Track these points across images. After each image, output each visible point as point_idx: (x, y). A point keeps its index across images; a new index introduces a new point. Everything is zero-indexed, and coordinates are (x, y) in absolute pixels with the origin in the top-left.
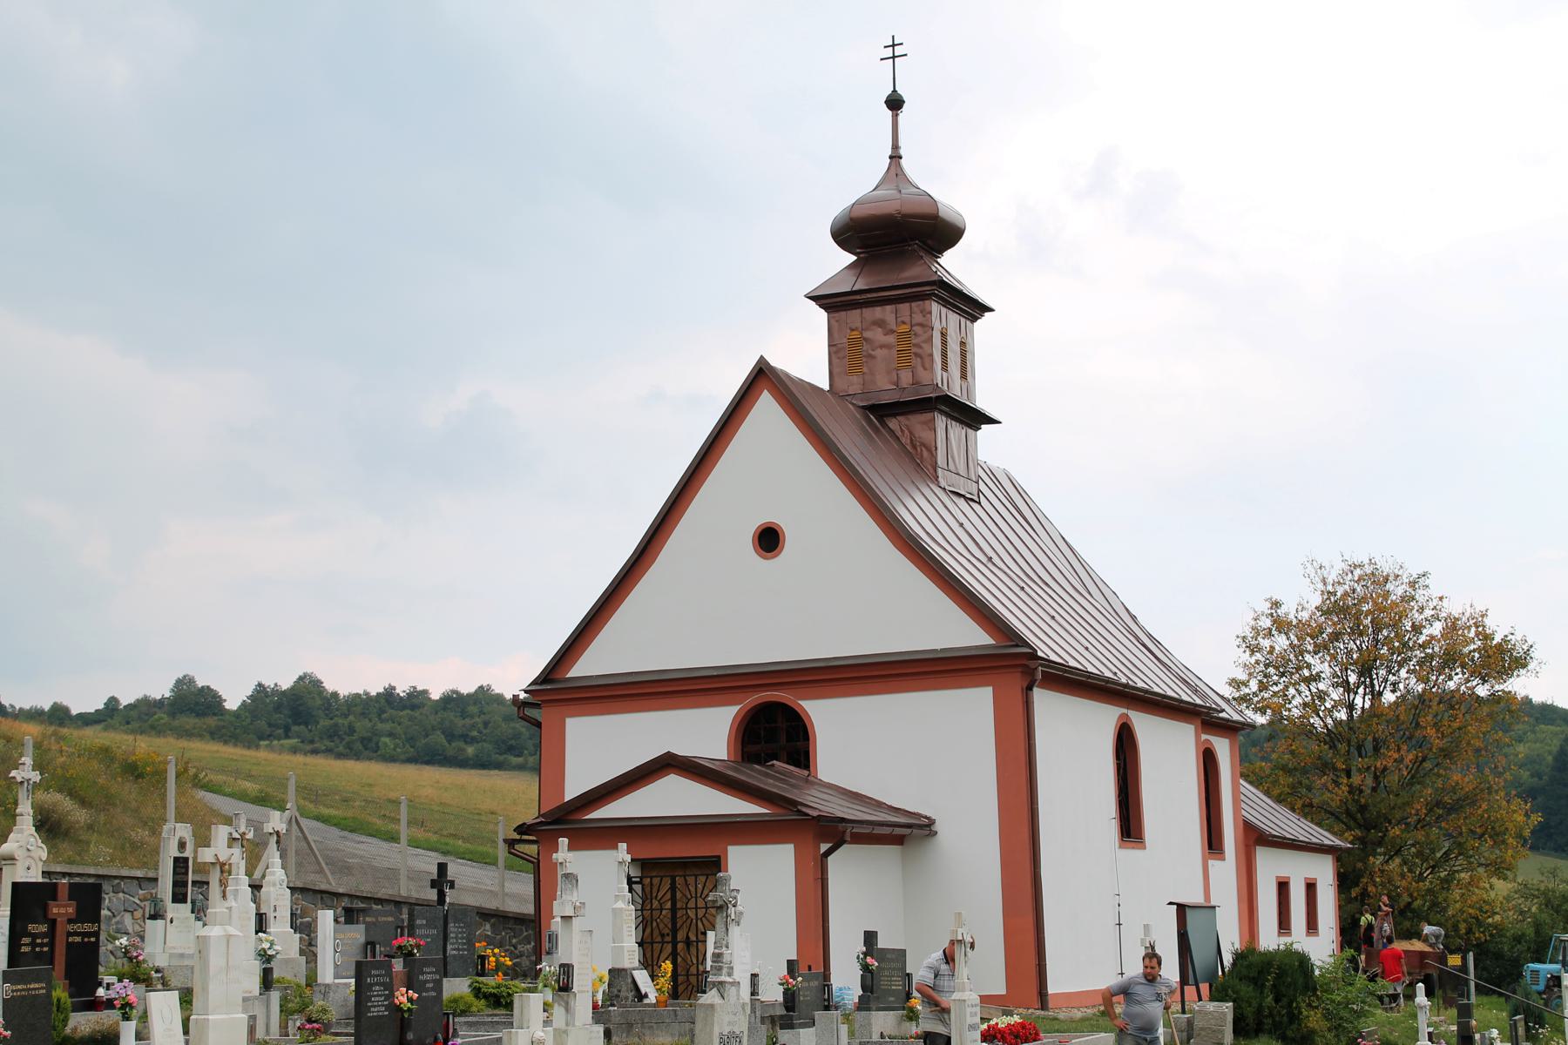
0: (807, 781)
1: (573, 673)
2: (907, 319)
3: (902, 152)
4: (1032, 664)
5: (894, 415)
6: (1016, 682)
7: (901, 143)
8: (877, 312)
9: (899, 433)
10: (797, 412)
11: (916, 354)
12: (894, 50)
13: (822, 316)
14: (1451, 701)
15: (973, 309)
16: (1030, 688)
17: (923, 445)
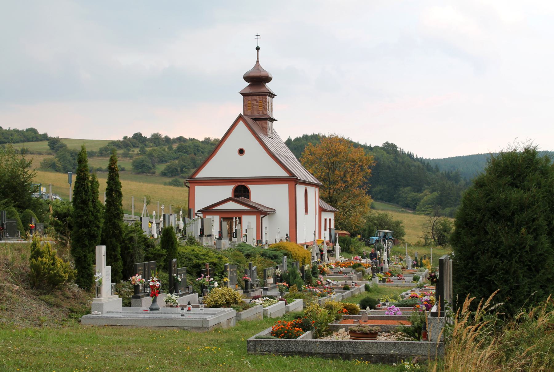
0: (249, 201)
1: (197, 177)
2: (261, 100)
3: (259, 60)
4: (297, 180)
5: (258, 120)
6: (294, 183)
7: (259, 58)
8: (255, 97)
9: (259, 125)
10: (247, 124)
11: (263, 108)
12: (258, 37)
13: (242, 97)
14: (518, 308)
15: (272, 95)
16: (296, 185)
17: (264, 127)
